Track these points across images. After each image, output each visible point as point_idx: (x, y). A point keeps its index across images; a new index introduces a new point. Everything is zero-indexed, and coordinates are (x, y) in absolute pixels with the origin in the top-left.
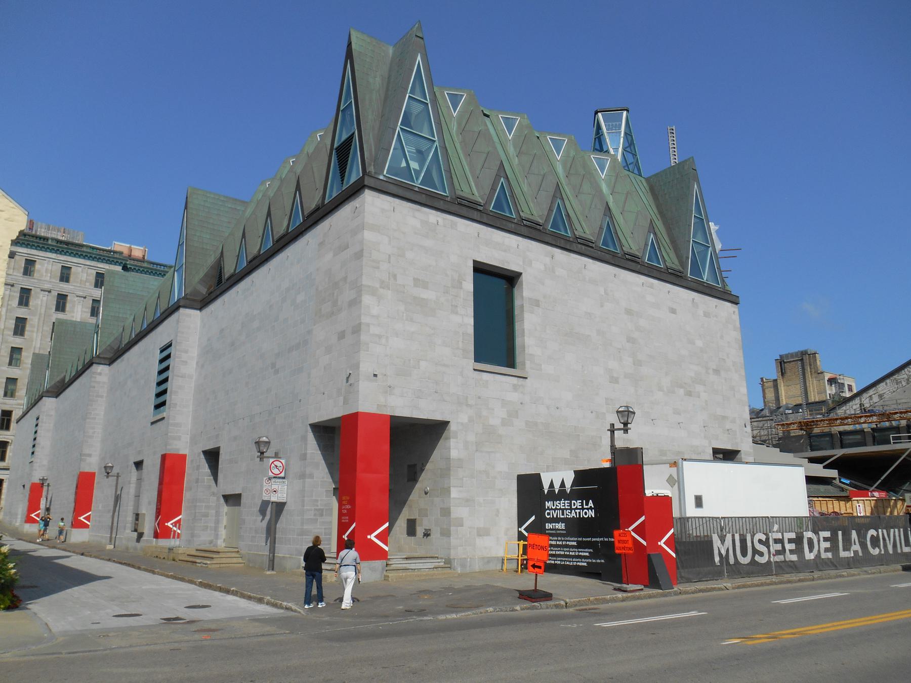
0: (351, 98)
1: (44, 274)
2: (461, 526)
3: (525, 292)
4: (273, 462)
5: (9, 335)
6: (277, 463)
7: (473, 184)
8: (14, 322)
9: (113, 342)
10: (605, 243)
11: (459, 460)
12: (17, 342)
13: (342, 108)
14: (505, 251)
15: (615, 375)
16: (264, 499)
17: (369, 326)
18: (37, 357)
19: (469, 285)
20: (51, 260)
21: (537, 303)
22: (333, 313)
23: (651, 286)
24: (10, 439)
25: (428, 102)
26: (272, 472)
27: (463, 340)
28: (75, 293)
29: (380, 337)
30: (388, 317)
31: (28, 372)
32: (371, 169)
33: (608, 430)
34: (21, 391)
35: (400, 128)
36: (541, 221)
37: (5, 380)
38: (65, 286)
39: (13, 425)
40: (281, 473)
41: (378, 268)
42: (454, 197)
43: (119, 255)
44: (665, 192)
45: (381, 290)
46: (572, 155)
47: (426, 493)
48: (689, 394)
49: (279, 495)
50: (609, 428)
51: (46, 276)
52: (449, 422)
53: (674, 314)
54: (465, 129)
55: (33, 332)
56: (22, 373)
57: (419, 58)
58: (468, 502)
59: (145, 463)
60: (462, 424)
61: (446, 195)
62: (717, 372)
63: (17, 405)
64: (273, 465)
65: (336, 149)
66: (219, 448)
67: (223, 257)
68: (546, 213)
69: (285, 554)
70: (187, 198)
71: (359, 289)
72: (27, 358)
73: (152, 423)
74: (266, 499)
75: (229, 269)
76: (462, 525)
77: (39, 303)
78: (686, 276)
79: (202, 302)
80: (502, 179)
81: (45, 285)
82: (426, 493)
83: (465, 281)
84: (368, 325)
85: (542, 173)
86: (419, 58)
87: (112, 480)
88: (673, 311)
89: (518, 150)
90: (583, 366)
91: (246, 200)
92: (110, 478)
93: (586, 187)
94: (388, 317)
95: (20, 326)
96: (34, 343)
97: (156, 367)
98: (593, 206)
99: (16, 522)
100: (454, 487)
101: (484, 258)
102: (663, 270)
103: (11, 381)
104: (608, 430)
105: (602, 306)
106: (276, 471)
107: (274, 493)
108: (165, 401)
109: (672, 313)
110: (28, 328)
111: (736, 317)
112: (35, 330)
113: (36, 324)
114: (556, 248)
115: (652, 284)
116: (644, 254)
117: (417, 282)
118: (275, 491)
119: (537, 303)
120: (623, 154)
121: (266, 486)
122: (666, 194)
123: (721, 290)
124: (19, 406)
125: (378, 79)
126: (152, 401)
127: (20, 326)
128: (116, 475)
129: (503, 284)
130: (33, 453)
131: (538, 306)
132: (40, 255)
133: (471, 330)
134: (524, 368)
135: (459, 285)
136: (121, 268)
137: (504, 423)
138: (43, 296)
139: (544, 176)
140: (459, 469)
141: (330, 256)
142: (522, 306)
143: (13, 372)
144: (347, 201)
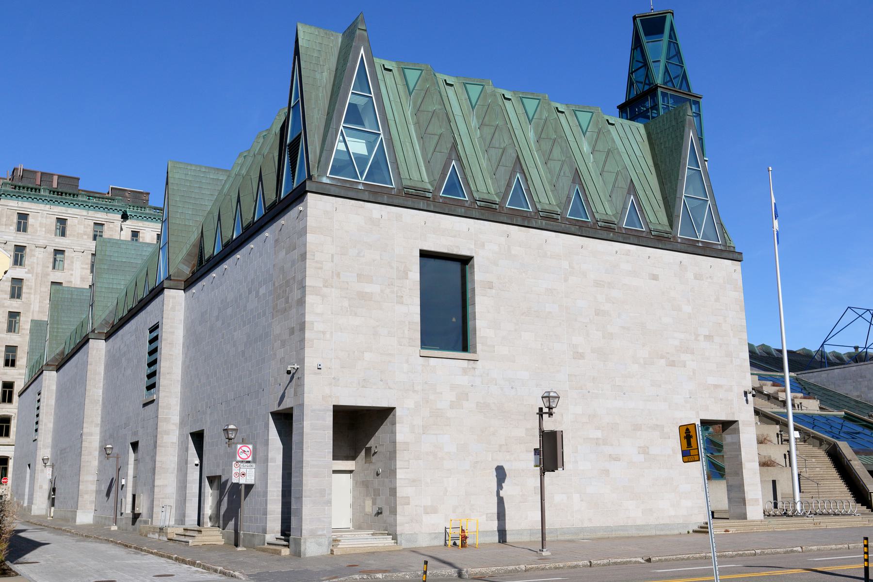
0: (299, 97)
1: (39, 229)
2: (407, 505)
3: (479, 275)
4: (240, 448)
5: (5, 299)
6: (245, 449)
7: (423, 169)
8: (10, 284)
9: (108, 315)
10: (574, 212)
11: (407, 443)
12: (15, 305)
13: (292, 104)
14: (455, 236)
15: (580, 351)
16: (233, 482)
17: (313, 324)
18: (37, 325)
19: (415, 275)
20: (44, 212)
21: (490, 286)
22: (285, 310)
23: (628, 253)
24: (13, 413)
25: (373, 95)
26: (240, 457)
27: (409, 328)
28: (73, 247)
29: (324, 333)
30: (332, 313)
31: (27, 338)
32: (314, 172)
33: (537, 414)
34: (22, 360)
35: (343, 126)
36: (497, 200)
37: (4, 349)
38: (61, 241)
39: (15, 397)
40: (249, 457)
41: (321, 268)
42: (401, 188)
43: (118, 202)
44: (662, 141)
45: (325, 289)
46: (544, 117)
47: (378, 474)
48: (672, 364)
49: (248, 478)
50: (538, 412)
51: (40, 231)
52: (395, 408)
53: (203, 434)
54: (420, 109)
55: (30, 293)
56: (21, 340)
57: (362, 51)
58: (414, 482)
59: (140, 444)
60: (408, 409)
61: (392, 187)
62: (709, 338)
63: (18, 376)
64: (241, 451)
65: (288, 146)
66: (203, 430)
67: (203, 237)
68: (503, 190)
69: (254, 532)
70: (168, 173)
71: (302, 287)
72: (25, 322)
73: (145, 405)
74: (236, 482)
75: (208, 252)
76: (408, 504)
77: (35, 261)
78: (675, 237)
79: (189, 284)
80: (454, 162)
81: (41, 241)
82: (378, 474)
83: (410, 271)
84: (312, 323)
85: (502, 147)
86: (362, 51)
87: (112, 460)
88: (655, 277)
89: (481, 121)
90: (542, 344)
91: (228, 169)
92: (111, 459)
93: (557, 153)
94: (332, 313)
95: (17, 288)
96: (32, 306)
97: (147, 348)
98: (562, 174)
99: (23, 503)
100: (401, 468)
101: (426, 247)
102: (644, 235)
103: (11, 350)
104: (537, 414)
105: (566, 280)
106: (244, 456)
107: (243, 476)
108: (155, 383)
109: (653, 279)
110: (25, 290)
111: (738, 276)
112: (33, 291)
113: (33, 284)
114: (452, 262)
115: (629, 251)
116: (621, 219)
117: (360, 277)
118: (243, 474)
119: (490, 286)
120: (666, 66)
121: (235, 470)
122: (661, 143)
123: (723, 248)
124: (20, 377)
125: (325, 74)
126: (145, 382)
127: (17, 288)
128: (116, 456)
129: (457, 266)
130: (36, 430)
131: (491, 288)
132: (32, 208)
133: (417, 318)
134: (475, 352)
135: (405, 275)
136: (120, 216)
137: (452, 406)
138: (39, 254)
139: (504, 149)
140: (405, 451)
141: (283, 252)
142: (473, 290)
143: (13, 339)
144: (294, 204)
